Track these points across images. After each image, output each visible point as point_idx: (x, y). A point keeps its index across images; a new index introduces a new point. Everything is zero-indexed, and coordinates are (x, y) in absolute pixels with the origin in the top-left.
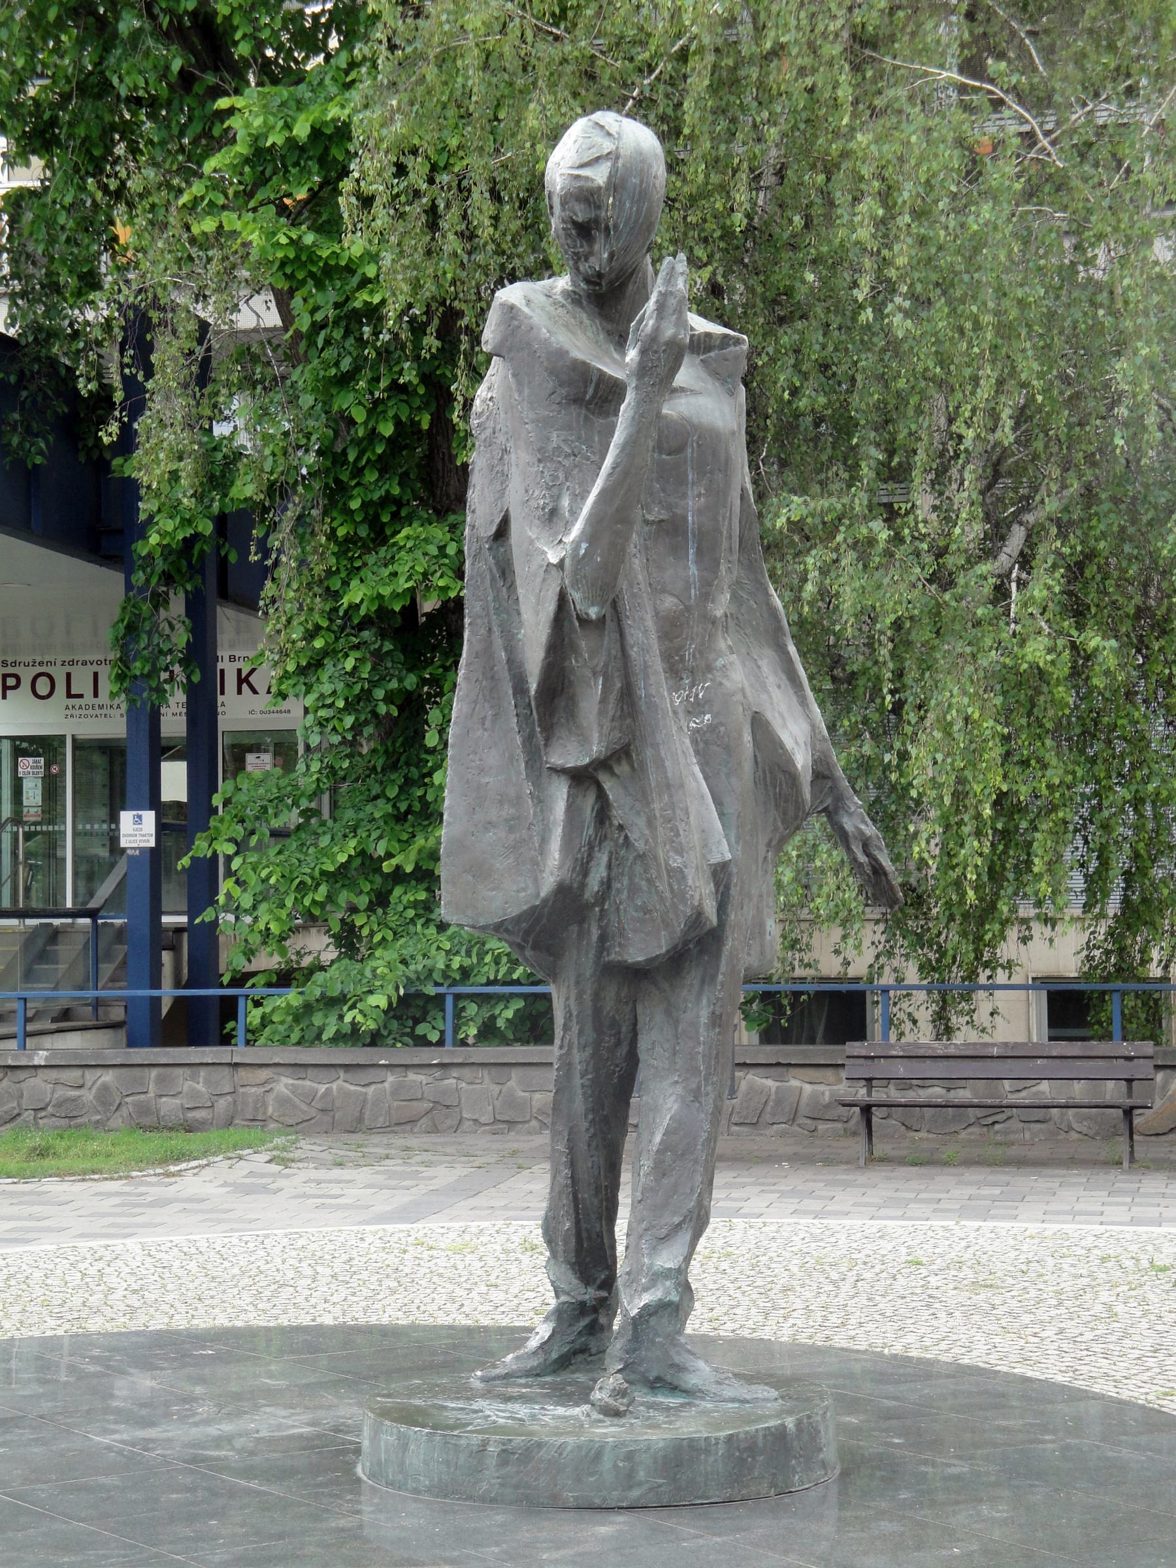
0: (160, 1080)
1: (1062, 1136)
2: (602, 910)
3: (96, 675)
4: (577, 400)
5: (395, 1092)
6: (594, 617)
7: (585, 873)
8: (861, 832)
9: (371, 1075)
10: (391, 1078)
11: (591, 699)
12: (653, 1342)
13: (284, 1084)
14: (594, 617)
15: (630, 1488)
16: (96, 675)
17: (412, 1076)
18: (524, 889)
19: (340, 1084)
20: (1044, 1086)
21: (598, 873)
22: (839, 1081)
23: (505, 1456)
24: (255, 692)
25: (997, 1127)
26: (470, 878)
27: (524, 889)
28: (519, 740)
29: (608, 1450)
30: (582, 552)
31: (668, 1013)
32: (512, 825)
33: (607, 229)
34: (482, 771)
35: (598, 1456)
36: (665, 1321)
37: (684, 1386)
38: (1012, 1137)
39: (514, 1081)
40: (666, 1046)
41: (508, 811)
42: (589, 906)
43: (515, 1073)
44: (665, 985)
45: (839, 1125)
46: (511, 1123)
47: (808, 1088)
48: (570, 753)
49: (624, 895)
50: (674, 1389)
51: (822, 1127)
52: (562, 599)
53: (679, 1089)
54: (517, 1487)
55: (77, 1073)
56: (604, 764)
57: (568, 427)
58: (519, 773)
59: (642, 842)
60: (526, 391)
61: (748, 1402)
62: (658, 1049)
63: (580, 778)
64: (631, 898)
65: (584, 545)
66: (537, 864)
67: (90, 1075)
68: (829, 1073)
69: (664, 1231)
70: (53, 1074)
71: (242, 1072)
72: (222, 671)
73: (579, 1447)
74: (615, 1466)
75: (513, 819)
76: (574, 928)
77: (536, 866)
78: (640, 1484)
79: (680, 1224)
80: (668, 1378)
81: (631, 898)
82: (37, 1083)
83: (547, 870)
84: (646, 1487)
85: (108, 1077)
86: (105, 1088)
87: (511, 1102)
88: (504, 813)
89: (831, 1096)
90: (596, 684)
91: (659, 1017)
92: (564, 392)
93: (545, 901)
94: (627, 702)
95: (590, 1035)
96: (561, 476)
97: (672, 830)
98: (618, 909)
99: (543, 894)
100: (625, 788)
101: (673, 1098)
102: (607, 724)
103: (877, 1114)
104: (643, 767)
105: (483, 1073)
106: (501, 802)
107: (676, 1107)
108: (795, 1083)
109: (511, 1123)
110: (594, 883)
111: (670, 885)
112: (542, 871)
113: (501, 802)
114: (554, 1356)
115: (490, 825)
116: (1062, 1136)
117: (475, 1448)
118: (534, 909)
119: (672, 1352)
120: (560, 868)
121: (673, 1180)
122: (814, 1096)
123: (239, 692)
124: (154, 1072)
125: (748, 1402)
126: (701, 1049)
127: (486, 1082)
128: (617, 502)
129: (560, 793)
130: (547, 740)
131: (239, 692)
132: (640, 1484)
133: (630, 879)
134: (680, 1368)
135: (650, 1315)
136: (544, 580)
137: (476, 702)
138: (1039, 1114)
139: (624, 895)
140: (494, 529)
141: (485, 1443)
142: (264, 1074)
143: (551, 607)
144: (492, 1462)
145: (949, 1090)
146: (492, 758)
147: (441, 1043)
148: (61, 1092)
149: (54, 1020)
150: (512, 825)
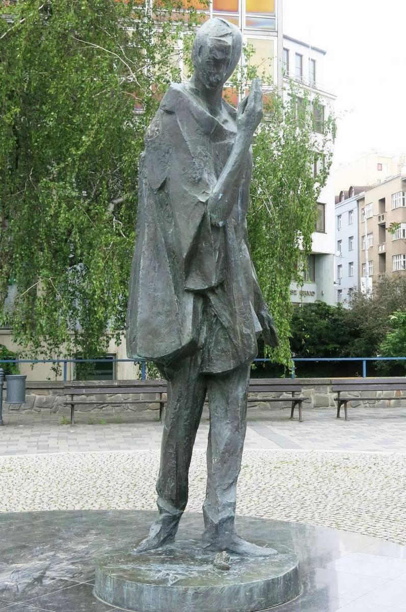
1: (125, 411)
2: (203, 351)
4: (207, 134)
6: (221, 226)
7: (199, 334)
8: (269, 317)
11: (212, 262)
12: (224, 534)
14: (221, 226)
15: (251, 603)
18: (174, 342)
21: (204, 335)
22: (49, 394)
23: (196, 595)
25: (104, 408)
26: (151, 337)
27: (174, 342)
28: (171, 277)
29: (242, 588)
30: (220, 197)
31: (222, 394)
32: (168, 313)
33: (228, 63)
34: (155, 290)
35: (238, 592)
36: (228, 524)
37: (238, 551)
38: (109, 412)
40: (222, 408)
41: (166, 308)
42: (198, 349)
44: (222, 383)
45: (49, 409)
47: (38, 397)
48: (195, 283)
49: (213, 344)
50: (232, 552)
51: (42, 410)
52: (204, 217)
53: (230, 426)
54: (202, 608)
56: (212, 290)
57: (203, 144)
58: (171, 291)
59: (227, 323)
60: (186, 128)
61: (267, 556)
62: (218, 409)
63: (200, 295)
64: (216, 345)
65: (221, 195)
66: (181, 331)
68: (46, 392)
69: (226, 486)
73: (230, 588)
74: (246, 595)
75: (169, 311)
76: (189, 359)
77: (180, 332)
78: (254, 601)
79: (232, 483)
80: (231, 548)
81: (216, 345)
83: (186, 334)
84: (257, 602)
88: (165, 309)
89: (46, 399)
90: (215, 254)
91: (218, 396)
92: (202, 129)
93: (183, 348)
94: (226, 264)
95: (190, 404)
96: (203, 165)
97: (245, 318)
98: (209, 351)
99: (183, 344)
100: (219, 299)
101: (227, 430)
102: (219, 272)
103: (76, 406)
104: (231, 290)
106: (164, 304)
107: (229, 433)
108: (33, 395)
110: (202, 340)
111: (242, 341)
112: (183, 334)
113: (164, 304)
114: (162, 538)
115: (159, 313)
116: (125, 411)
117: (181, 592)
118: (178, 350)
119: (233, 536)
120: (192, 332)
121: (228, 465)
122: (40, 400)
125: (267, 556)
126: (239, 409)
128: (236, 177)
129: (189, 303)
130: (186, 277)
132: (254, 601)
133: (216, 338)
134: (235, 544)
135: (223, 523)
136: (194, 209)
137: (151, 260)
139: (213, 344)
140: (159, 186)
141: (186, 590)
143: (198, 221)
144: (189, 598)
145: (72, 395)
146: (159, 285)
150: (168, 313)
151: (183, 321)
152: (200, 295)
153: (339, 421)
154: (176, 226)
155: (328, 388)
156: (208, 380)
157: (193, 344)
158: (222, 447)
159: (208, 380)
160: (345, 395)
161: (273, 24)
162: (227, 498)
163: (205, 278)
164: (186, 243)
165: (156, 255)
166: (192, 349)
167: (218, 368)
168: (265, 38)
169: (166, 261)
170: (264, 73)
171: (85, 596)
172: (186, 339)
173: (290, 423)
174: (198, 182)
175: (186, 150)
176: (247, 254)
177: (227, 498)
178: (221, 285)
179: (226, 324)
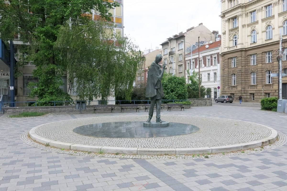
0: (29, 109)
3: (1, 74)
5: (50, 110)
9: (48, 108)
10: (50, 109)
11: (159, 85)
13: (41, 109)
16: (1, 74)
17: (52, 108)
19: (45, 109)
20: (100, 108)
24: (5, 75)
39: (61, 109)
43: (61, 108)
46: (60, 112)
48: (156, 88)
52: (158, 80)
55: (21, 109)
56: (158, 89)
67: (22, 109)
70: (19, 109)
71: (37, 108)
72: (218, 49)
77: (155, 94)
82: (17, 110)
85: (24, 109)
86: (24, 110)
87: (60, 110)
105: (58, 108)
109: (60, 112)
123: (3, 75)
124: (28, 109)
127: (58, 109)
129: (155, 90)
131: (3, 75)
138: (100, 110)
142: (39, 108)
147: (35, 106)
148: (19, 110)
149: (213, 115)
151: (155, 93)
152: (157, 89)
153: (145, 112)
154: (154, 80)
155: (141, 106)
156: (157, 100)
157: (156, 95)
158: (158, 109)
159: (157, 100)
160: (146, 107)
161: (121, 26)
162: (159, 115)
163: (158, 87)
164: (156, 83)
165: (151, 84)
166: (156, 96)
167: (158, 98)
168: (119, 29)
169: (153, 85)
170: (129, 41)
171: (14, 154)
172: (155, 95)
173: (121, 113)
174: (158, 75)
175: (156, 71)
176: (286, 109)
177: (159, 115)
178: (160, 88)
179: (160, 93)
